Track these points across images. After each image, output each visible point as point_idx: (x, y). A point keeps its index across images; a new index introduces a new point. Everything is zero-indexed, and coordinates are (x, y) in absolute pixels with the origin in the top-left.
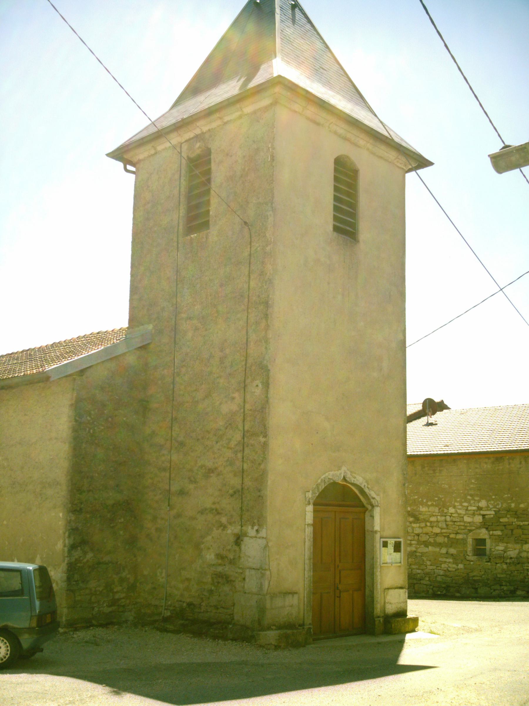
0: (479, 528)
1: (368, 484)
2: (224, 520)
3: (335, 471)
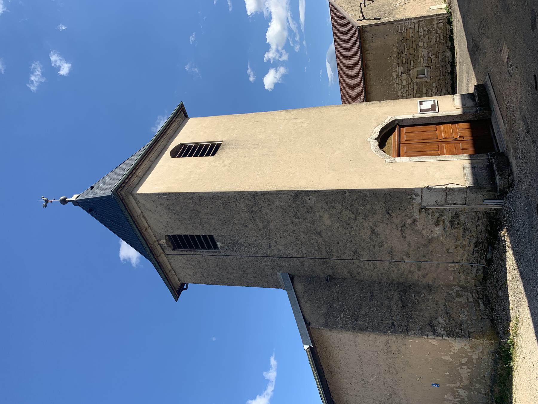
0: (409, 75)
2: (409, 221)
3: (370, 145)
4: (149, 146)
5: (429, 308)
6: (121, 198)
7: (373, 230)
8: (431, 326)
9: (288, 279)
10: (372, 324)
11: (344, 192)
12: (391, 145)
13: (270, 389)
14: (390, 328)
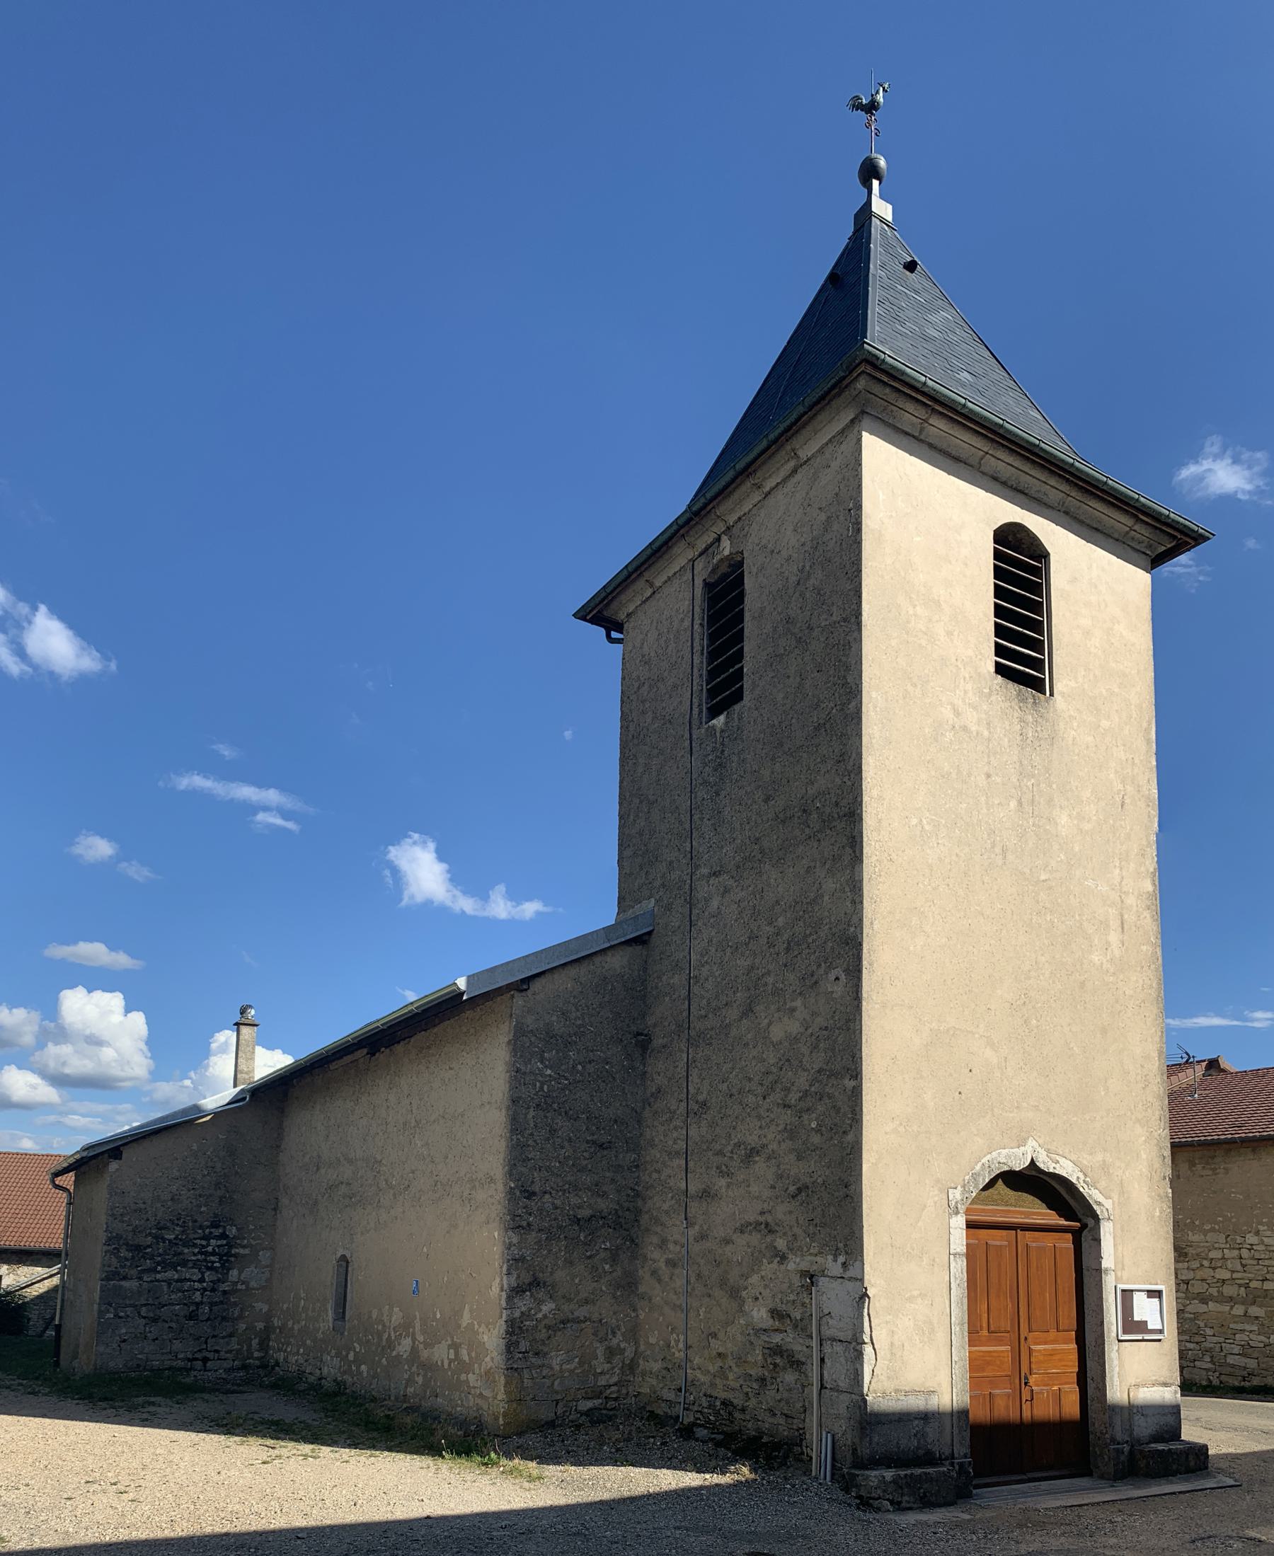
1: (1086, 1175)
2: (781, 1244)
4: (1034, 445)
5: (577, 1281)
6: (845, 383)
7: (758, 1153)
8: (530, 1284)
9: (637, 930)
10: (529, 1146)
11: (855, 1073)
12: (1015, 1206)
13: (467, 905)
14: (523, 1186)
